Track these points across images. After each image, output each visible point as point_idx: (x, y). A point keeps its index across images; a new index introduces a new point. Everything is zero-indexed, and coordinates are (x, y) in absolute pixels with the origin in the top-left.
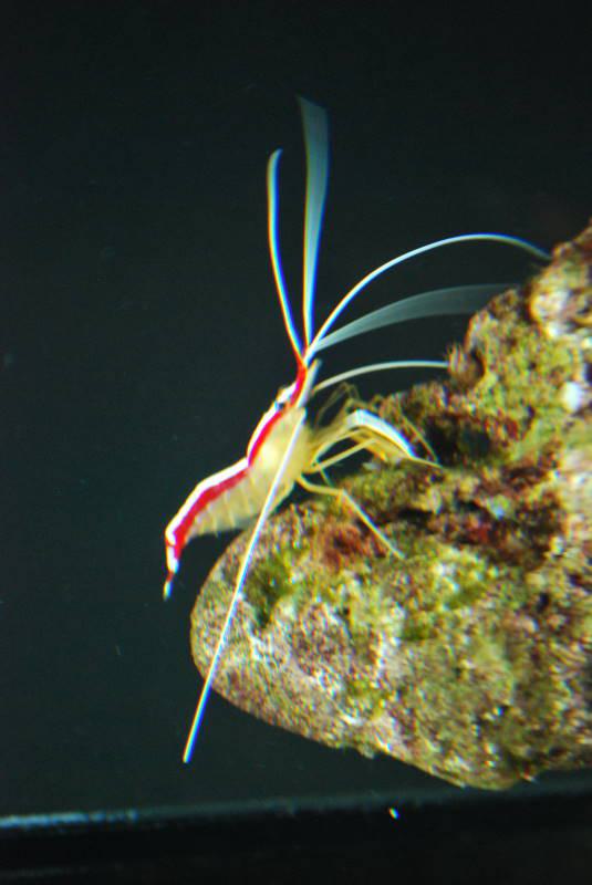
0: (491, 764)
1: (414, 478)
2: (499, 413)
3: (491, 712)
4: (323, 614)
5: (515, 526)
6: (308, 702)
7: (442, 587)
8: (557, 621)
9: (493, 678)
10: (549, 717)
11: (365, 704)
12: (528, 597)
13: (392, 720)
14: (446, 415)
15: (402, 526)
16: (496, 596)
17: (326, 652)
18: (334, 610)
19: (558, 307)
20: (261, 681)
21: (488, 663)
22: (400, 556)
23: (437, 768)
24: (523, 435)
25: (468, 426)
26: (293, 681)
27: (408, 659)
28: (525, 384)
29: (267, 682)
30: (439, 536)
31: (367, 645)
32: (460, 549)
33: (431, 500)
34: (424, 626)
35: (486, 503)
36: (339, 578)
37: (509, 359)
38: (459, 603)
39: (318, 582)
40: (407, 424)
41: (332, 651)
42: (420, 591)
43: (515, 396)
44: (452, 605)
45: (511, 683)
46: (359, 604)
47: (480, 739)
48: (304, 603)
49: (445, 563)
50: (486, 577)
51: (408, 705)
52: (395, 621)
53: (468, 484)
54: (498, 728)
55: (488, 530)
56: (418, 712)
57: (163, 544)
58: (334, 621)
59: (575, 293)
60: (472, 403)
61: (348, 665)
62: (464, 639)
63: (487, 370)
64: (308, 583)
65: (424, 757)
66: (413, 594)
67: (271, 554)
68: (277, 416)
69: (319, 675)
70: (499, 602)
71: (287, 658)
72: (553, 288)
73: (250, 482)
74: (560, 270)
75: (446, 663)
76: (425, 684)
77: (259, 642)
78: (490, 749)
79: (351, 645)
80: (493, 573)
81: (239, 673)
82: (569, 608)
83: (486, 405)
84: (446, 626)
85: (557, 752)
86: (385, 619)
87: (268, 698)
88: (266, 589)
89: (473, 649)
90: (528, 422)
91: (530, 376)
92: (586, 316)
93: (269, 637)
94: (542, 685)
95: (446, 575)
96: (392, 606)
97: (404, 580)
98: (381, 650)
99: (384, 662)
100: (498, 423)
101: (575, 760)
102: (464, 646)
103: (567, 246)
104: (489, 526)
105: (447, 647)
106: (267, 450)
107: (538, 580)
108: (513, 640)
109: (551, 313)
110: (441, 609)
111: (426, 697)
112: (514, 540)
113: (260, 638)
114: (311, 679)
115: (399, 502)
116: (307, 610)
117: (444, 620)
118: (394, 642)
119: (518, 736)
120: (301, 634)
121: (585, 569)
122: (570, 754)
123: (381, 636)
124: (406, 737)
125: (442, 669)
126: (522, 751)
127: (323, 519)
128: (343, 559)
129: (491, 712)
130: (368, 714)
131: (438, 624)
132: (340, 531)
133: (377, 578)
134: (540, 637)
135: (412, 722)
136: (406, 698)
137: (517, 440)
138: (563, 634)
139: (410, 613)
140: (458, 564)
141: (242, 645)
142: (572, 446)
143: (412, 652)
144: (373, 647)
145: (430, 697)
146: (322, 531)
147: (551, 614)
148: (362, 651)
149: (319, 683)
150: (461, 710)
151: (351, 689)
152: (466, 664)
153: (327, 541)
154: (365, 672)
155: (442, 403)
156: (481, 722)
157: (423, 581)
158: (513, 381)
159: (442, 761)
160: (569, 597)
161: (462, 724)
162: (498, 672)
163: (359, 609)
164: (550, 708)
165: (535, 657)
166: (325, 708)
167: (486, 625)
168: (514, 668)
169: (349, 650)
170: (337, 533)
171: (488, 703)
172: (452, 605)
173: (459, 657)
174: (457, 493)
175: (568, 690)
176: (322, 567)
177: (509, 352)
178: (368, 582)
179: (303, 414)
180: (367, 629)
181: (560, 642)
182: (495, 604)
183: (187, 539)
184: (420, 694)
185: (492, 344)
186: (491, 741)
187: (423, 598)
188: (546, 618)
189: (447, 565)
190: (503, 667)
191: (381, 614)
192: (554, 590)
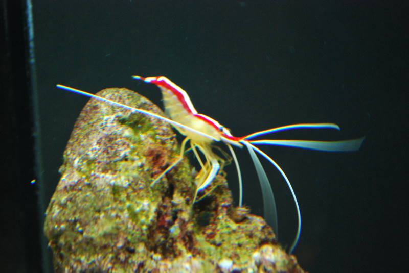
0: (56, 226)
1: (188, 191)
2: (218, 230)
3: (80, 227)
4: (125, 149)
5: (166, 237)
6: (85, 142)
7: (138, 204)
8: (122, 257)
9: (95, 228)
10: (78, 253)
11: (84, 168)
12: (133, 244)
13: (76, 181)
14: (217, 206)
15: (166, 185)
16: (134, 229)
17: (108, 150)
18: (127, 154)
19: (267, 257)
20: (94, 120)
21: (103, 225)
22: (152, 184)
23: (54, 201)
24: (208, 241)
25: (212, 216)
26: (95, 135)
27: (104, 188)
28: (232, 242)
29: (94, 123)
30: (161, 202)
31: (111, 169)
32: (155, 212)
33: (178, 199)
34: (120, 196)
35: (177, 224)
36: (142, 156)
37: (243, 235)
38: (130, 212)
39: (140, 146)
40: (213, 188)
41: (108, 153)
42: (136, 194)
43: (226, 237)
44: (129, 208)
45: (93, 236)
46: (130, 166)
47: (67, 221)
48: (130, 140)
49: (149, 205)
50: (143, 224)
51: (83, 188)
52: (122, 183)
53: (185, 216)
54: (73, 230)
55: (164, 226)
56: (80, 193)
57: (158, 75)
58: (122, 154)
59: (274, 265)
60: (223, 217)
61: (102, 160)
62: (114, 214)
63: (238, 225)
64: (140, 142)
65: (59, 196)
66: (135, 191)
67: (153, 125)
68: (216, 128)
69: (97, 147)
70: (130, 230)
71: (105, 132)
72: (276, 255)
73: (186, 115)
74: (285, 258)
75: (103, 206)
76: (93, 196)
77: (112, 119)
78: (63, 226)
79: (111, 162)
80: (144, 227)
81: (98, 110)
82: (128, 262)
83: (222, 224)
84: (120, 206)
85: (62, 257)
86: (123, 178)
87: (86, 124)
88: (137, 123)
89: (109, 218)
90: (214, 243)
91: (235, 244)
92: (263, 270)
93: (115, 124)
94: (92, 250)
95: (143, 206)
96: (129, 180)
97: (141, 186)
98: (109, 176)
99: (103, 177)
100: (214, 230)
101: (58, 265)
102: (111, 214)
103: (296, 262)
104: (166, 226)
105: (110, 206)
106: (201, 122)
107: (141, 248)
108: (113, 236)
109: (264, 255)
110: (128, 203)
111: (87, 196)
112: (159, 237)
113: (114, 120)
114: (95, 144)
115: (177, 184)
116: (127, 142)
117: (122, 205)
118: (113, 182)
119: (69, 239)
120: (116, 139)
121: (146, 270)
122: (61, 263)
123: (115, 176)
124: (68, 187)
125: (100, 204)
126: (62, 241)
127: (169, 149)
128: (151, 158)
129: (80, 227)
130: (79, 170)
131: (121, 202)
132: (164, 157)
133: (142, 174)
134: (115, 249)
135: (75, 190)
136: (86, 187)
137: (206, 238)
138: (116, 260)
139: (126, 189)
140: (148, 211)
141: (111, 111)
142: (203, 264)
143: (108, 190)
144: (110, 172)
145: (87, 198)
146: (163, 149)
147: (125, 254)
148: (108, 167)
149: (94, 147)
150: (81, 213)
151: (91, 162)
152: (102, 215)
153: (159, 151)
154: (98, 169)
155: (223, 204)
156: (75, 222)
157: (141, 195)
158: (233, 236)
159: (58, 204)
160: (133, 263)
161: (74, 213)
162: (98, 230)
163: (128, 165)
164: (82, 254)
165: (105, 247)
166: (82, 150)
167: (120, 224)
168: (100, 237)
169: (108, 161)
170: (163, 155)
171: (84, 225)
172: (129, 208)
173: (105, 211)
174: (181, 211)
175: (90, 262)
176: (147, 148)
177: (246, 235)
178: (140, 170)
179: (218, 140)
180: (119, 169)
181: (112, 258)
182: (130, 228)
183: (160, 86)
184: (88, 194)
185: (250, 227)
186: (67, 226)
187: (132, 195)
188: (124, 252)
189: (148, 206)
190: (101, 232)
191: (125, 176)
192: (137, 255)
